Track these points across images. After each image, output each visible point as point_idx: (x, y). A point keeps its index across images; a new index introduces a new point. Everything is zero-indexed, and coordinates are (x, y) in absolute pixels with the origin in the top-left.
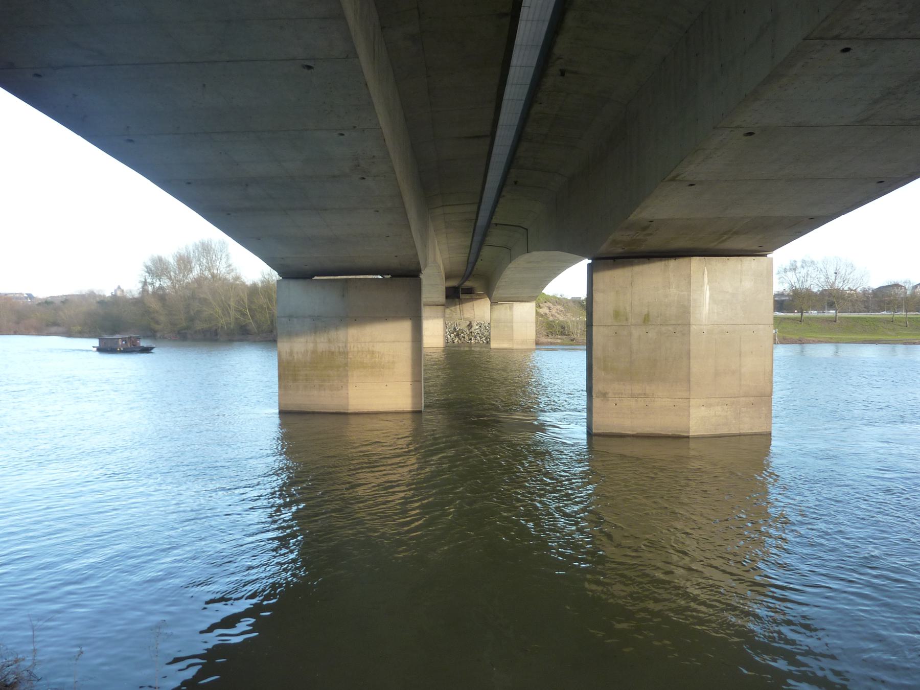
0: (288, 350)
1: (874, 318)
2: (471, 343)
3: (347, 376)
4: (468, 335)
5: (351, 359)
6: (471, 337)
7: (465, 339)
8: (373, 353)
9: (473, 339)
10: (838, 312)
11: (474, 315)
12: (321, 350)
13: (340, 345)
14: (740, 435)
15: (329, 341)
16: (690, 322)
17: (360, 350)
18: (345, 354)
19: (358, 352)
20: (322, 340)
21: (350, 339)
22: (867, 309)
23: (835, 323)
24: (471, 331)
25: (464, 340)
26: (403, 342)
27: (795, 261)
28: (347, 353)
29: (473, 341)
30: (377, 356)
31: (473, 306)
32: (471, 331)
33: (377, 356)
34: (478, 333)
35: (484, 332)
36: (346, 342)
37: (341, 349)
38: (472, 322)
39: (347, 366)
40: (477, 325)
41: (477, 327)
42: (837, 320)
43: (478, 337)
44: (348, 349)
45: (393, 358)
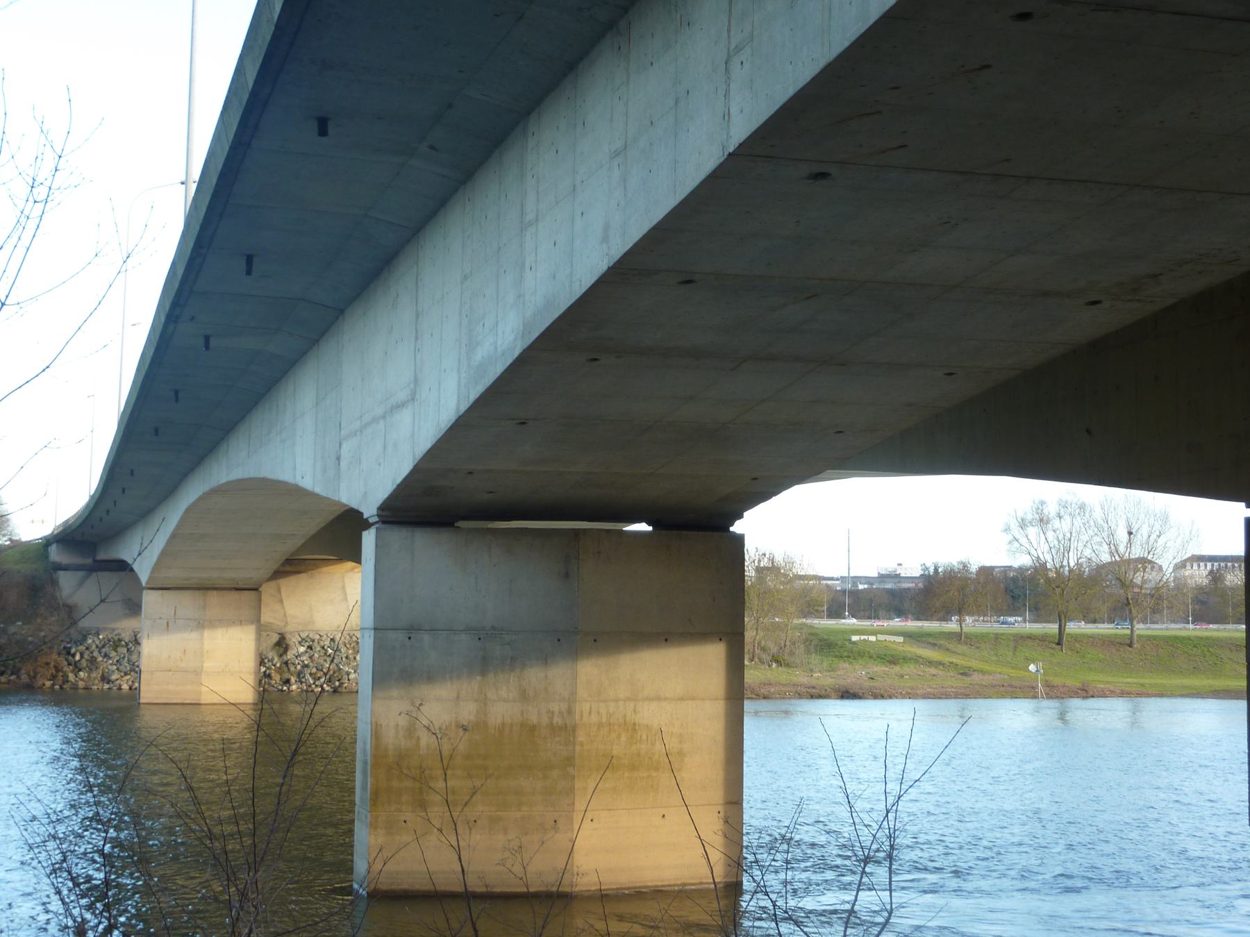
0: (403, 721)
1: (1208, 638)
2: (290, 691)
3: (571, 791)
4: (279, 671)
5: (582, 744)
6: (286, 676)
7: (273, 682)
8: (634, 728)
9: (293, 680)
10: (1135, 622)
11: (285, 615)
12: (499, 721)
13: (555, 707)
14: (468, 897)
15: (524, 696)
16: (375, 632)
17: (604, 720)
18: (566, 730)
19: (600, 725)
20: (503, 693)
21: (582, 692)
22: (1201, 617)
23: (1130, 649)
24: (285, 658)
25: (269, 684)
26: (703, 699)
27: (1042, 503)
28: (574, 729)
29: (294, 687)
30: (644, 737)
31: (279, 590)
32: (285, 658)
33: (644, 737)
34: (307, 666)
35: (321, 661)
36: (572, 699)
37: (557, 720)
38: (288, 636)
39: (573, 765)
40: (300, 643)
41: (302, 649)
42: (1135, 641)
43: (308, 676)
44: (577, 717)
45: (681, 742)
